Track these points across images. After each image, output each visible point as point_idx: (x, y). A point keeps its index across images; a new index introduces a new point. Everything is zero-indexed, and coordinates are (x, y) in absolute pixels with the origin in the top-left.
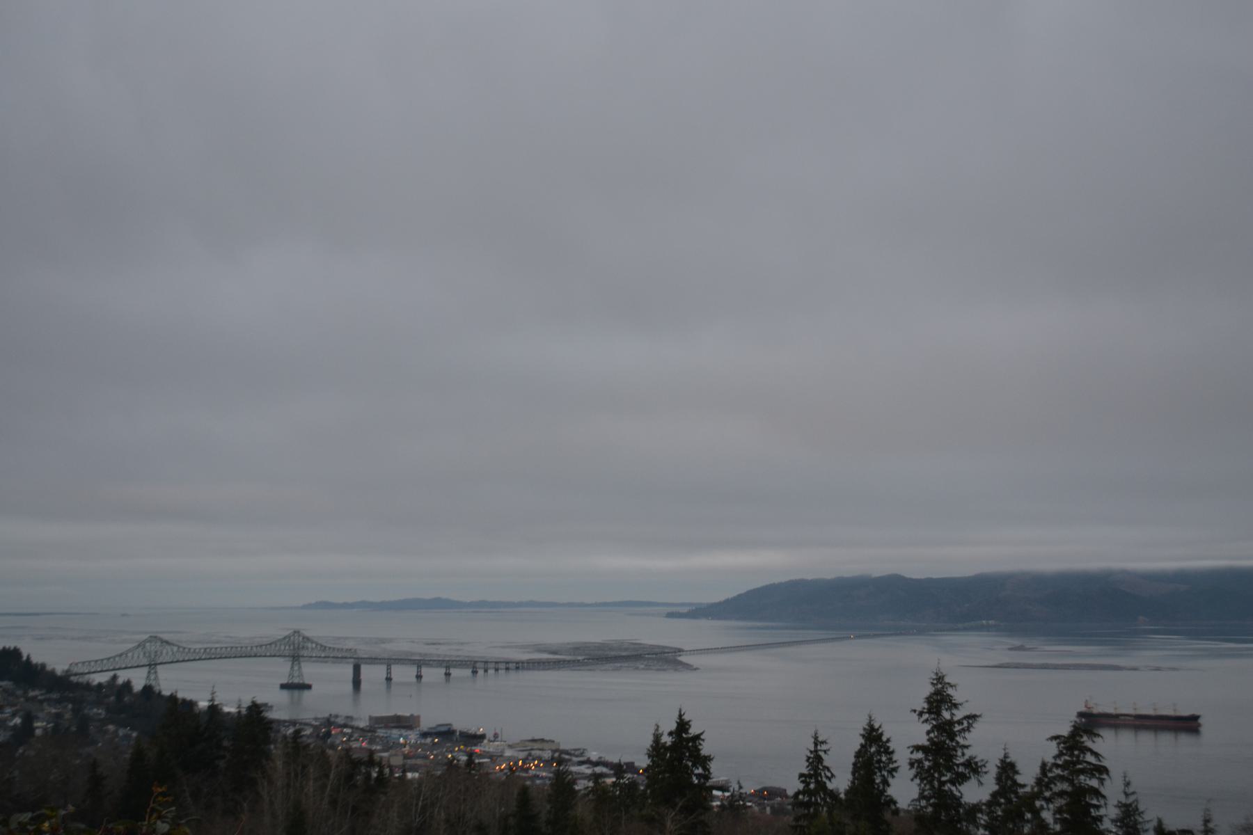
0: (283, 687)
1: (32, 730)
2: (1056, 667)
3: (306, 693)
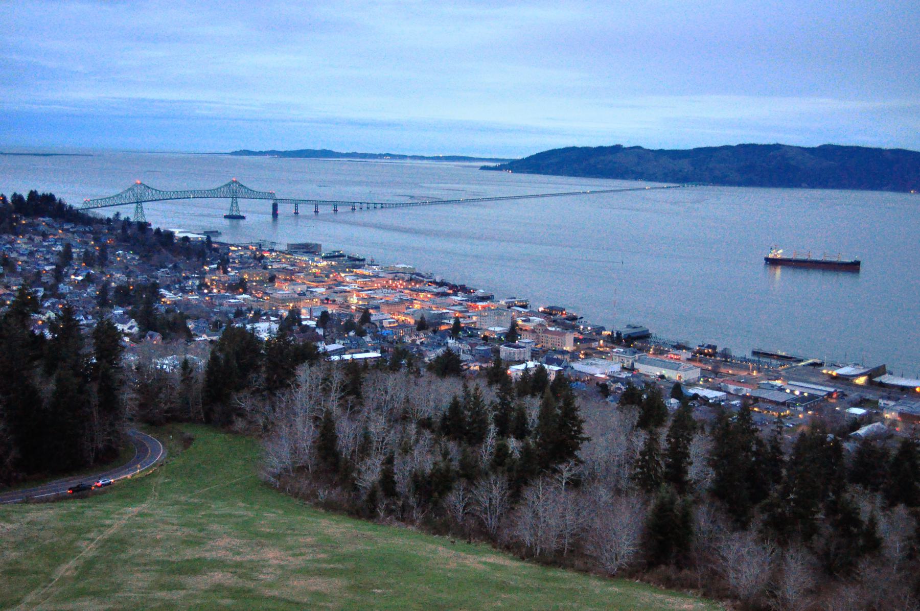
0: (226, 217)
3: (241, 222)
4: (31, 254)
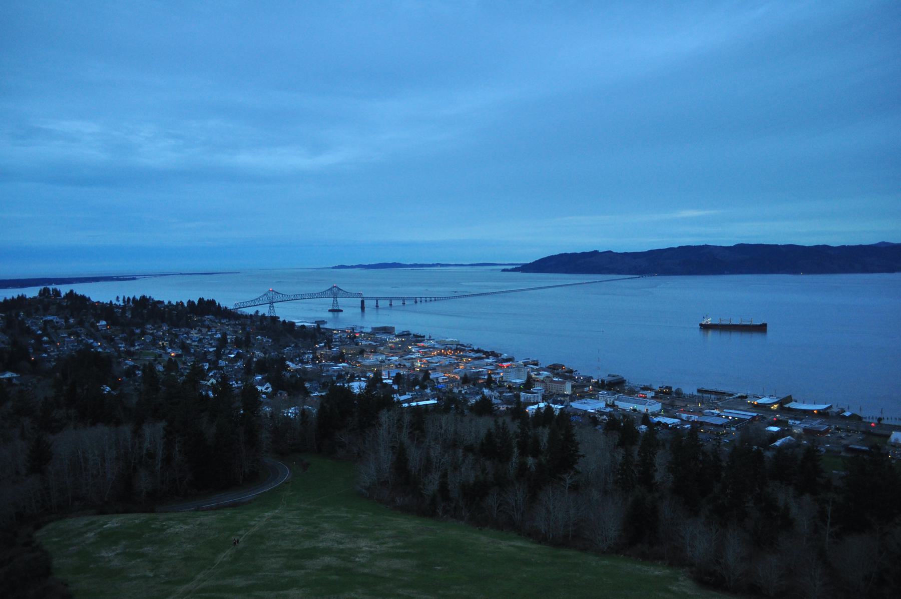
1: (227, 339)
2: (456, 265)
3: (340, 313)
4: (200, 340)
